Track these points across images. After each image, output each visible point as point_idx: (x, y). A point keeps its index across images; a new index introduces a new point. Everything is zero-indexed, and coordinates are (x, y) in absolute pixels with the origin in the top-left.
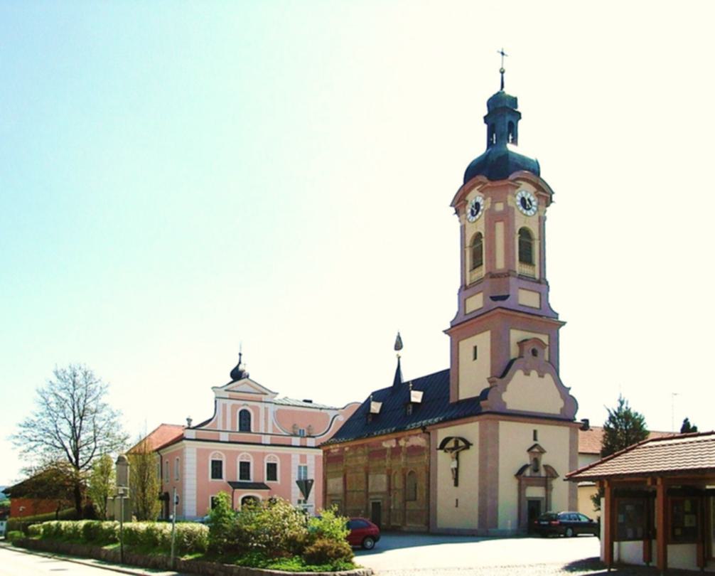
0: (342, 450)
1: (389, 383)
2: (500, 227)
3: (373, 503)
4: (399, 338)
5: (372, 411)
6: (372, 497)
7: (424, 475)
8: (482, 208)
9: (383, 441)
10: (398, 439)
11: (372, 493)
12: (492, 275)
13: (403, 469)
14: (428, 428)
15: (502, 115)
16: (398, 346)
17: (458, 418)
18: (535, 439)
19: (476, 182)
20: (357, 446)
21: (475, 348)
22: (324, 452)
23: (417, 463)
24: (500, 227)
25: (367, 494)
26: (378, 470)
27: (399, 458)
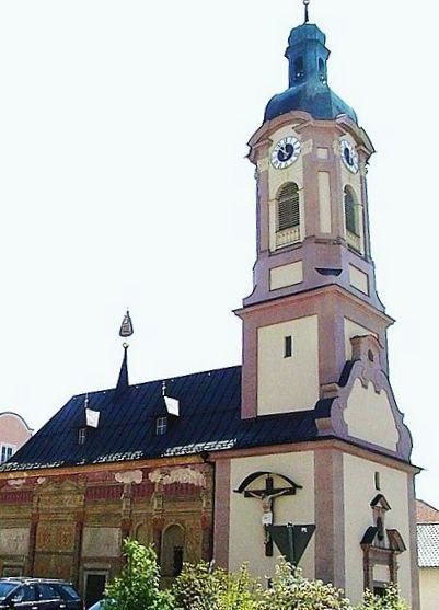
0: (31, 481)
1: (112, 383)
2: (323, 178)
3: (89, 576)
4: (128, 317)
5: (88, 424)
6: (87, 565)
7: (200, 535)
8: (296, 151)
9: (117, 472)
10: (146, 472)
11: (88, 560)
12: (314, 239)
13: (156, 521)
14: (212, 456)
15: (305, 50)
16: (127, 330)
17: (260, 444)
19: (291, 118)
20: (62, 478)
21: (288, 340)
23: (187, 515)
24: (323, 178)
25: (79, 559)
26: (105, 519)
27: (150, 503)
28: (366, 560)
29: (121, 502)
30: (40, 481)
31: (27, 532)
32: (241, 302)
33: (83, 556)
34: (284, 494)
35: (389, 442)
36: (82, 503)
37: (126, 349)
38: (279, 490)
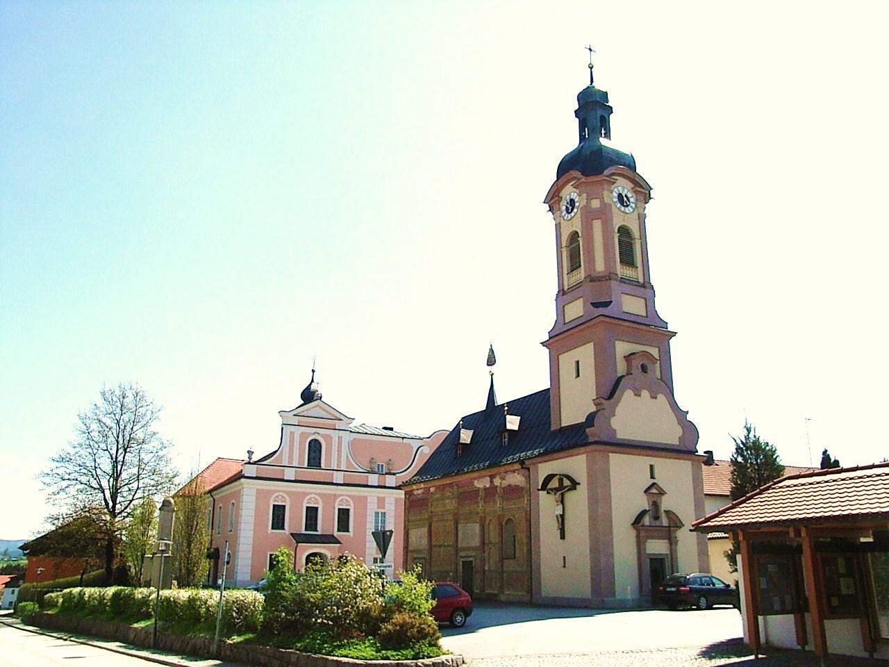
1: (482, 406)
2: (597, 225)
4: (492, 351)
6: (462, 554)
8: (577, 204)
9: (475, 479)
10: (492, 477)
11: (463, 549)
12: (592, 279)
14: (527, 462)
15: (593, 110)
16: (491, 361)
17: (562, 449)
18: (652, 477)
25: (457, 550)
27: (495, 502)
28: (638, 537)
29: (477, 503)
30: (432, 490)
31: (425, 530)
32: (548, 334)
33: (459, 546)
34: (567, 491)
35: (672, 436)
36: (456, 505)
37: (492, 375)
38: (566, 487)
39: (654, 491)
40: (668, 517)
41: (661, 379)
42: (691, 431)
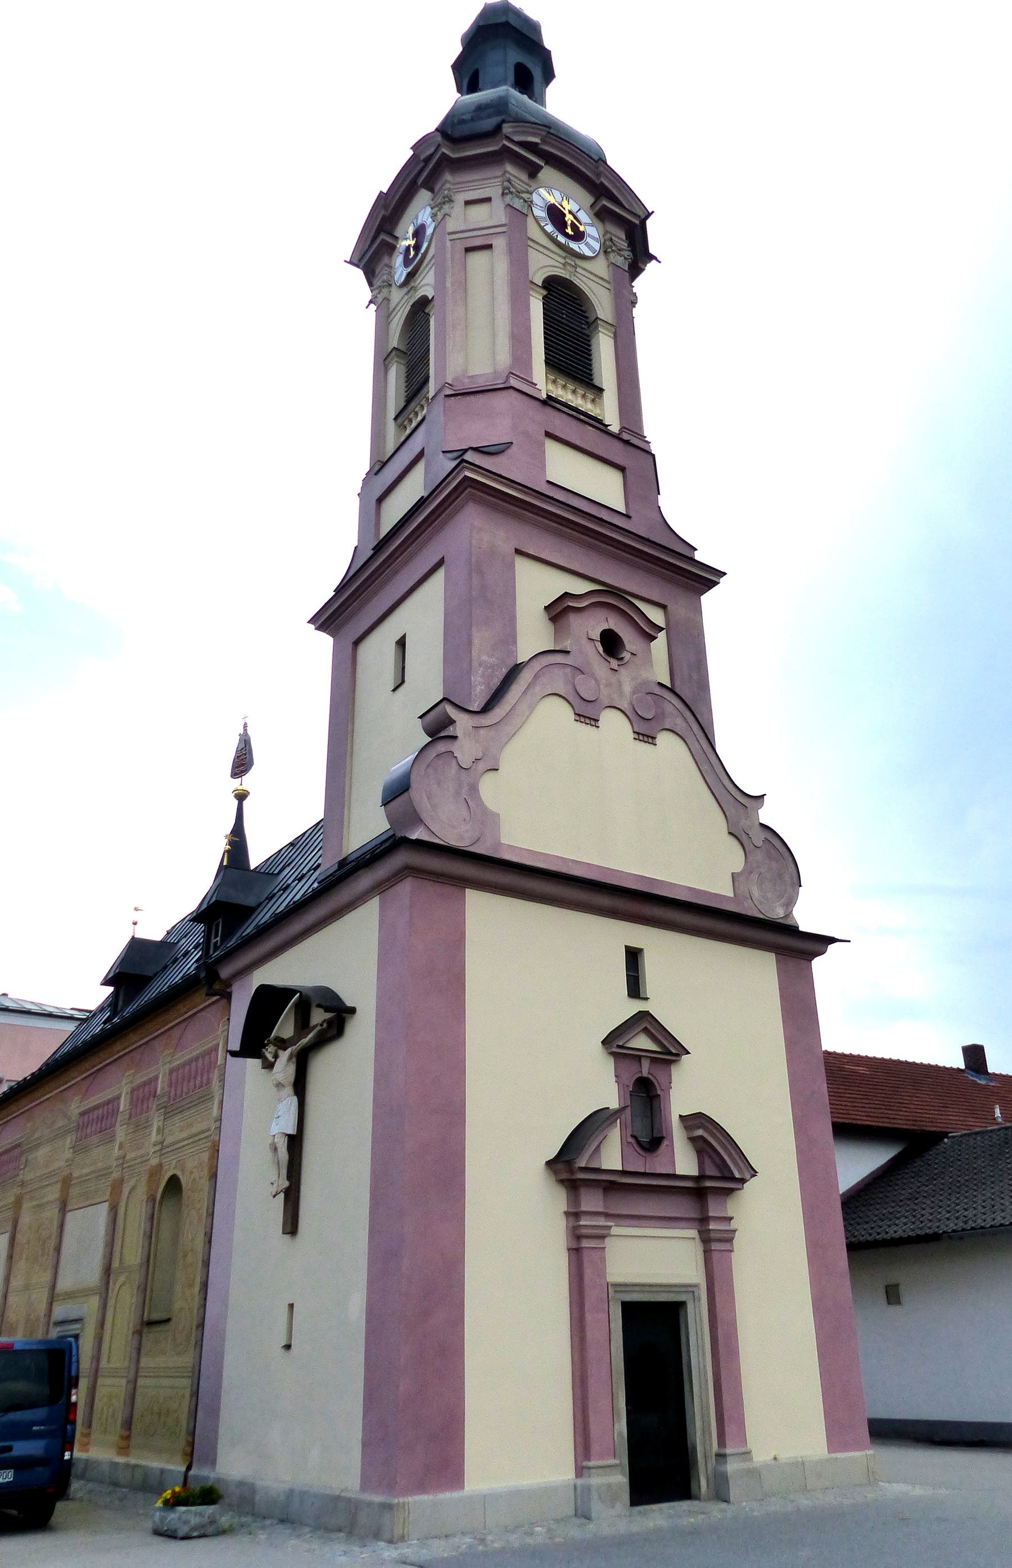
16: (242, 764)
18: (635, 988)
22: (580, 1206)
35: (705, 866)
39: (642, 1042)
40: (702, 1148)
41: (671, 690)
42: (773, 857)
